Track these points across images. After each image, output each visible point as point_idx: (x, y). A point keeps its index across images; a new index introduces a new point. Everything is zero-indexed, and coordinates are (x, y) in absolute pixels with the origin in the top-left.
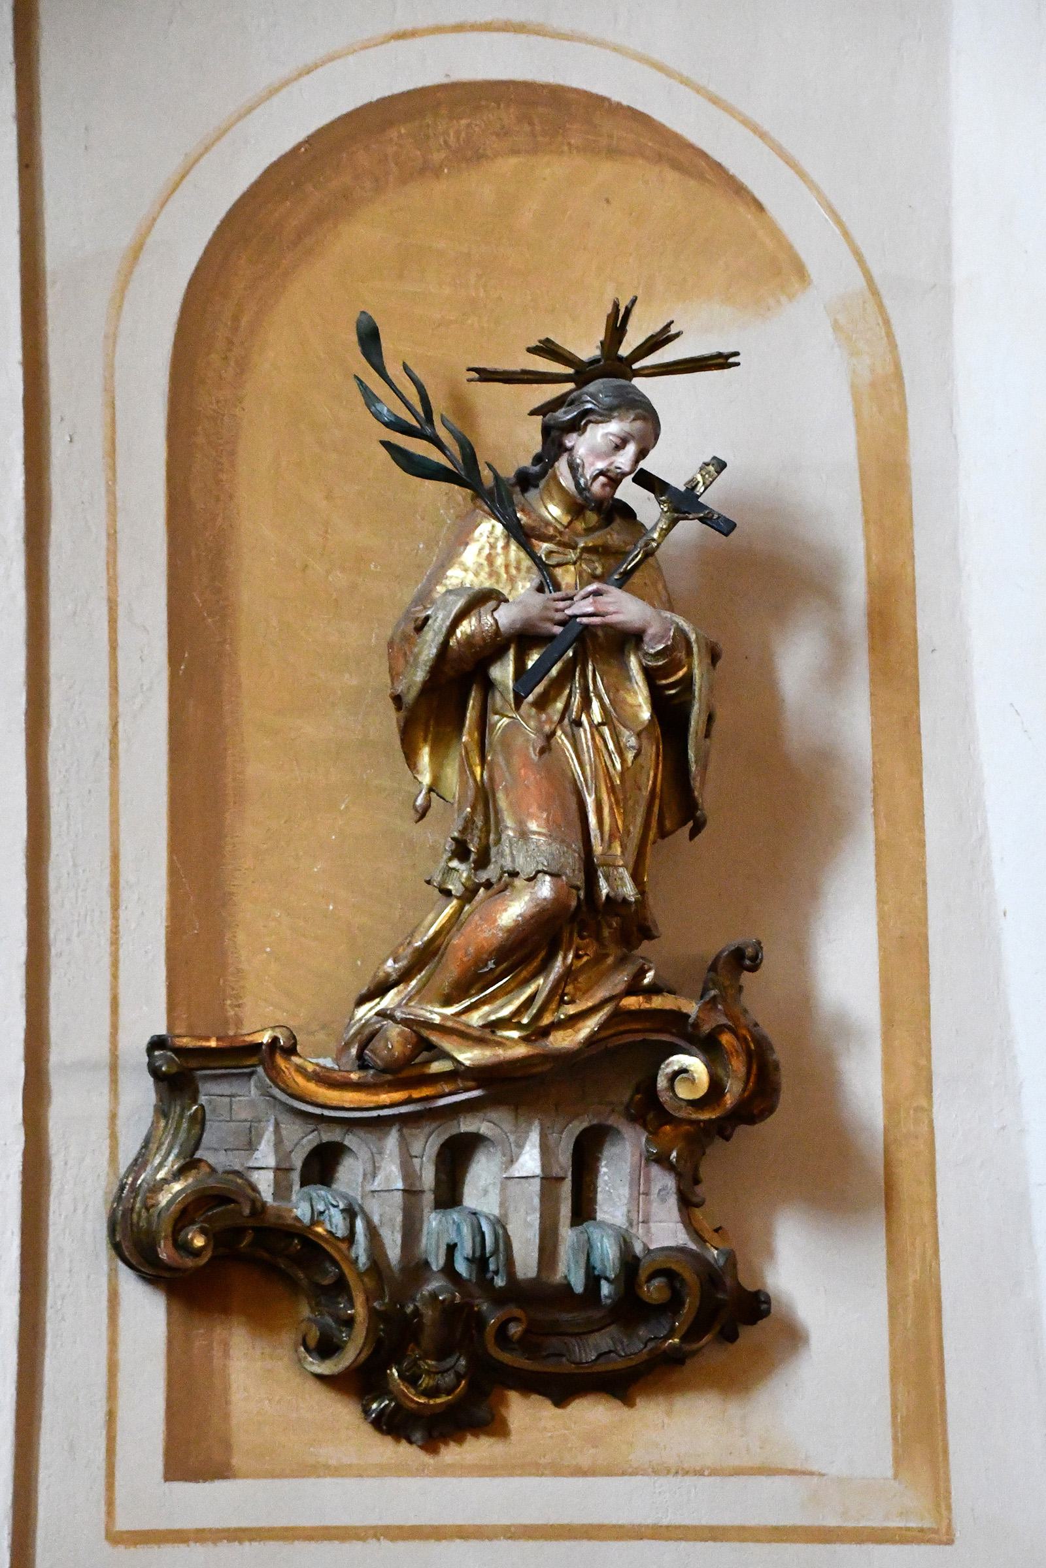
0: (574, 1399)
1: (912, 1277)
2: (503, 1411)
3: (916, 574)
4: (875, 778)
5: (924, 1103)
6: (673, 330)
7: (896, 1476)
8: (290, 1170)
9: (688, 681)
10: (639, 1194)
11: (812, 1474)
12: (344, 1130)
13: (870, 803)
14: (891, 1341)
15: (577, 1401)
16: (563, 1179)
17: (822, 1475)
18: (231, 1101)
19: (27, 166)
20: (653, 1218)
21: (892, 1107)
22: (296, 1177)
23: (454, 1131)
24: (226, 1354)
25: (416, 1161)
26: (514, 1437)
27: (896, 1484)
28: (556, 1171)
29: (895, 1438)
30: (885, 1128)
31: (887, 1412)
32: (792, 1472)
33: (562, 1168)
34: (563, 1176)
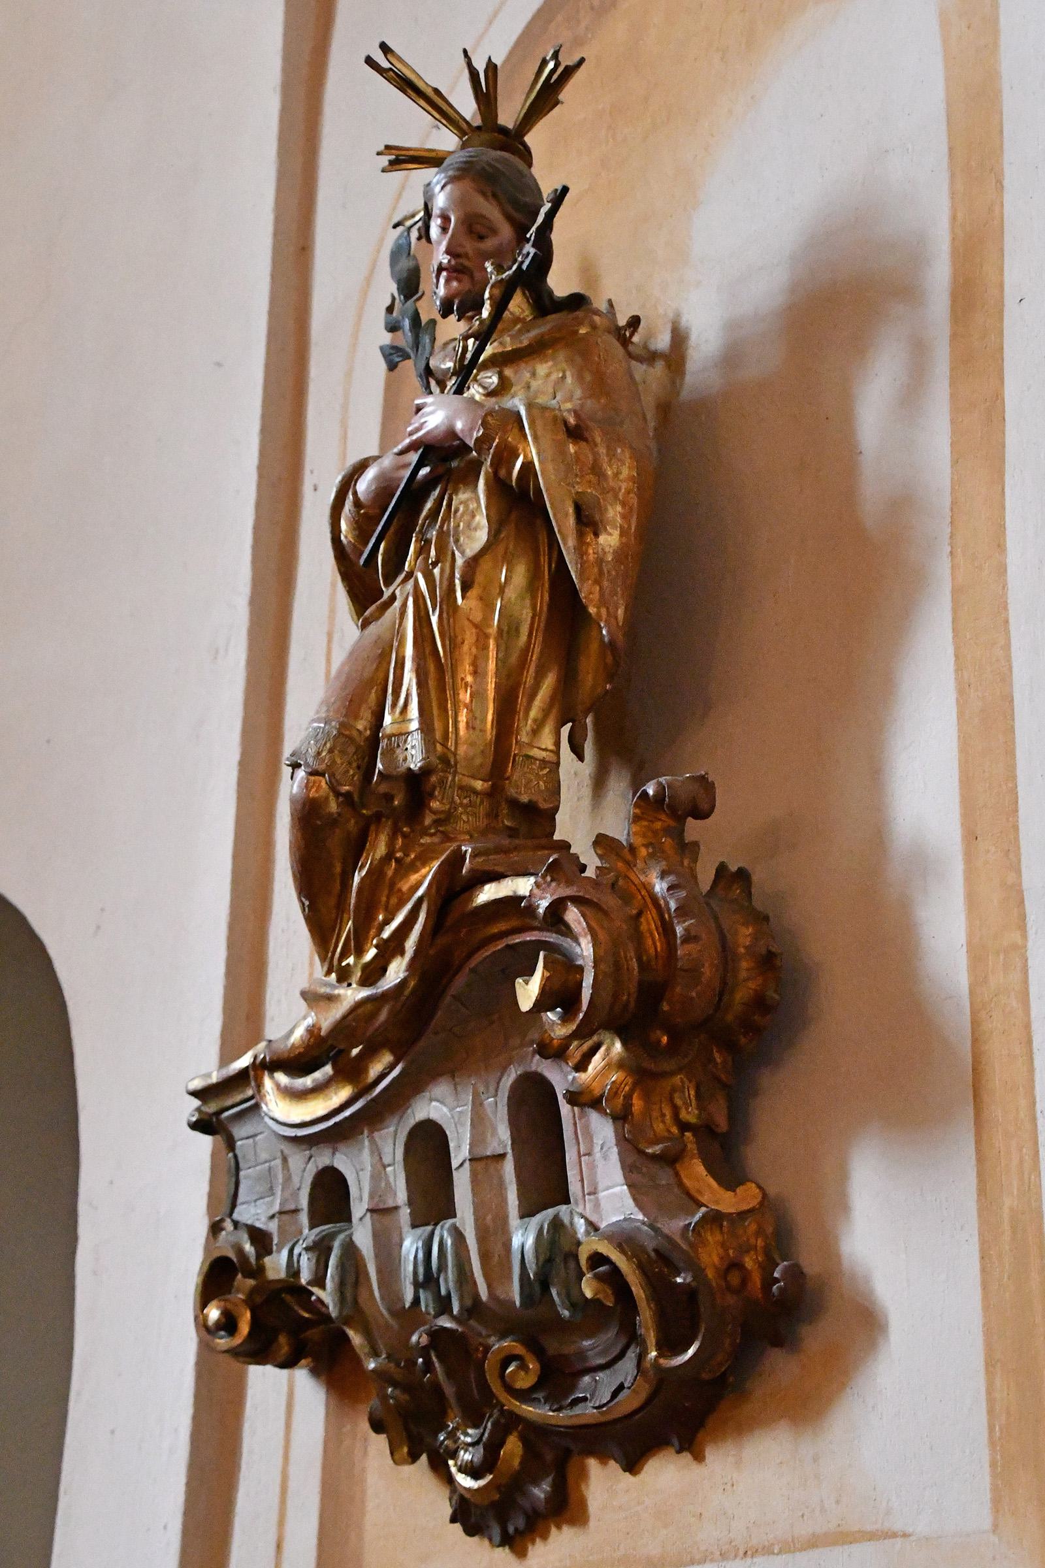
0: (647, 1461)
1: (1008, 1202)
2: (583, 1487)
3: (1005, 212)
4: (954, 503)
5: (1016, 937)
6: (567, 60)
7: (995, 1527)
8: (296, 1211)
9: (528, 466)
10: (580, 1157)
11: (894, 1535)
12: (331, 1150)
13: (947, 540)
14: (986, 1307)
15: (650, 1461)
16: (502, 1156)
17: (905, 1535)
18: (254, 1141)
19: (303, 249)
20: (601, 1186)
21: (977, 956)
22: (304, 1218)
23: (412, 1122)
24: (365, 1453)
25: (389, 1169)
26: (592, 1523)
27: (994, 1539)
28: (492, 1148)
29: (993, 1465)
30: (970, 988)
31: (981, 1418)
32: (872, 1536)
33: (501, 1142)
34: (502, 1152)
